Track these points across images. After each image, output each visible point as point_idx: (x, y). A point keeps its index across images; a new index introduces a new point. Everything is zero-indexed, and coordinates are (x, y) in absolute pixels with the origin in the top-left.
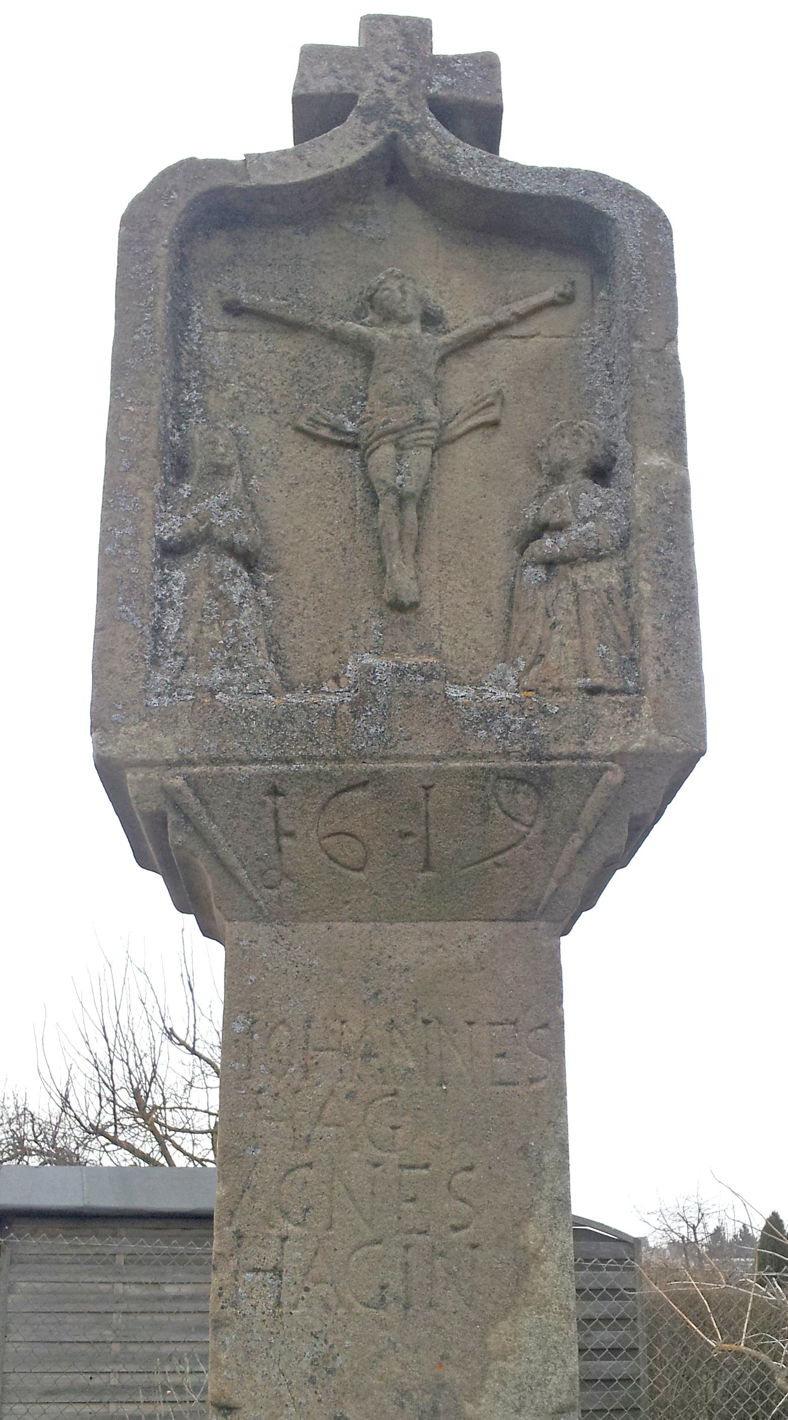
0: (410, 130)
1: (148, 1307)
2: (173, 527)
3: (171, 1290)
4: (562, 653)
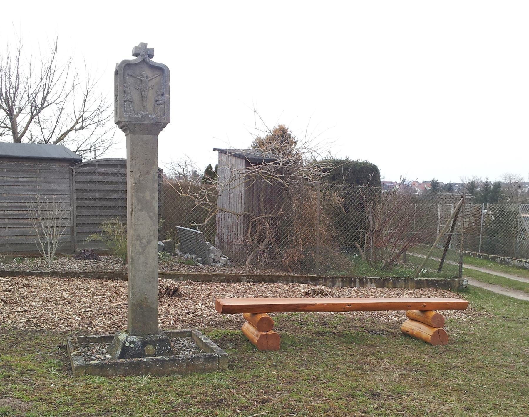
0: (146, 58)
1: (15, 184)
2: (125, 99)
3: (21, 179)
4: (159, 113)
